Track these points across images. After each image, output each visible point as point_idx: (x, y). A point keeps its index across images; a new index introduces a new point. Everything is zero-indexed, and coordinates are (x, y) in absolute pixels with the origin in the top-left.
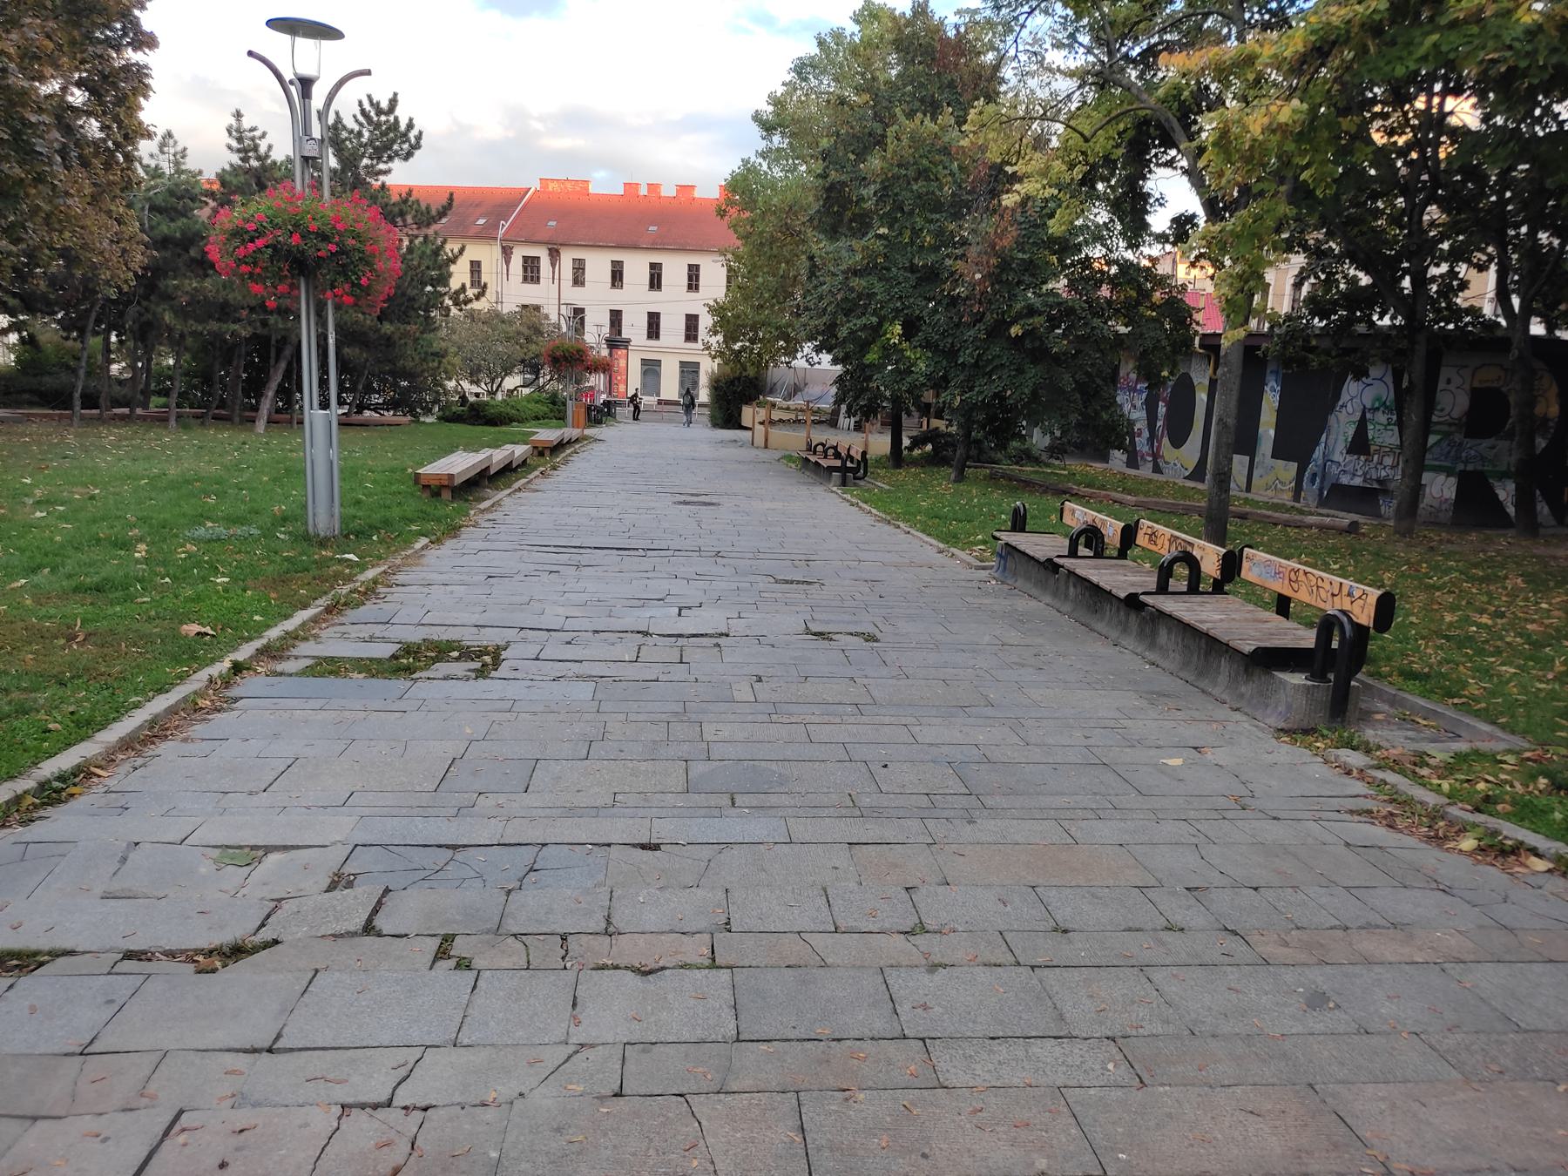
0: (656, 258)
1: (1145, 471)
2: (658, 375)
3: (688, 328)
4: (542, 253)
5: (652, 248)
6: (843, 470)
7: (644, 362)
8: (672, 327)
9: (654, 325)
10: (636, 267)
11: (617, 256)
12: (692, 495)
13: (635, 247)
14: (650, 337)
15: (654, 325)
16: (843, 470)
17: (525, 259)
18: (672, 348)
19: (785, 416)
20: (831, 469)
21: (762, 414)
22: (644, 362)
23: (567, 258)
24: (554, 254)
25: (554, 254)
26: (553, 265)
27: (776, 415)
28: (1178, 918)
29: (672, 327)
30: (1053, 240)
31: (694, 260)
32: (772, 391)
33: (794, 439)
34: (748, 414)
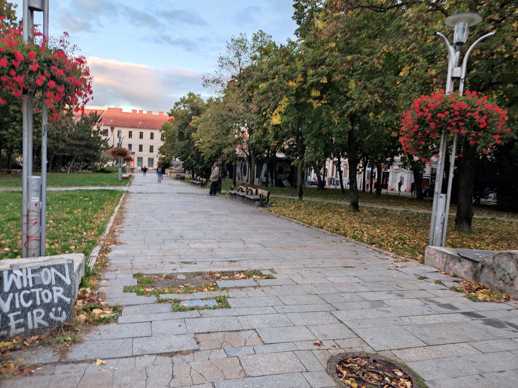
0: (142, 131)
1: (241, 181)
2: (142, 161)
3: (150, 149)
4: (109, 129)
5: (140, 128)
6: (202, 184)
7: (138, 158)
8: (146, 149)
9: (141, 148)
10: (136, 133)
11: (131, 130)
12: (446, 198)
13: (124, 127)
14: (150, 152)
15: (141, 148)
16: (202, 184)
17: (107, 130)
18: (146, 154)
19: (175, 171)
20: (199, 184)
21: (169, 171)
22: (138, 158)
23: (116, 130)
24: (112, 129)
25: (112, 129)
26: (112, 131)
27: (172, 171)
28: (36, 266)
29: (146, 149)
30: (326, 134)
31: (152, 131)
32: (172, 166)
33: (174, 175)
34: (167, 171)
